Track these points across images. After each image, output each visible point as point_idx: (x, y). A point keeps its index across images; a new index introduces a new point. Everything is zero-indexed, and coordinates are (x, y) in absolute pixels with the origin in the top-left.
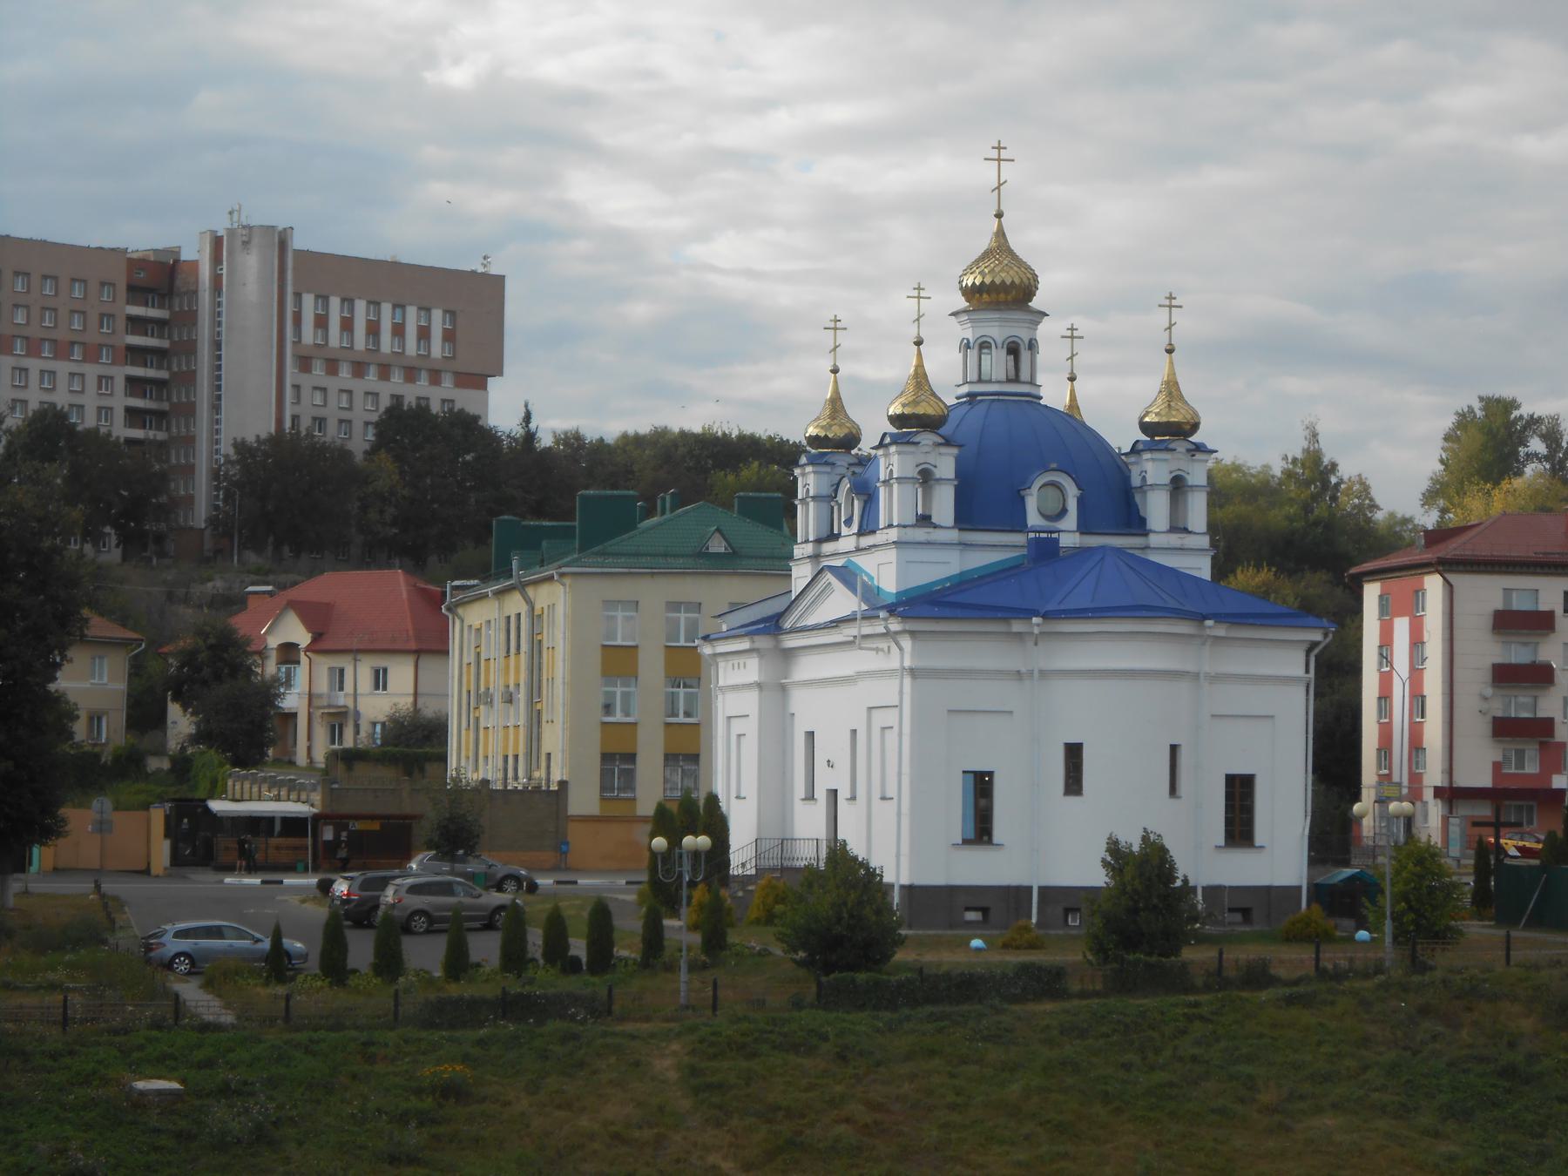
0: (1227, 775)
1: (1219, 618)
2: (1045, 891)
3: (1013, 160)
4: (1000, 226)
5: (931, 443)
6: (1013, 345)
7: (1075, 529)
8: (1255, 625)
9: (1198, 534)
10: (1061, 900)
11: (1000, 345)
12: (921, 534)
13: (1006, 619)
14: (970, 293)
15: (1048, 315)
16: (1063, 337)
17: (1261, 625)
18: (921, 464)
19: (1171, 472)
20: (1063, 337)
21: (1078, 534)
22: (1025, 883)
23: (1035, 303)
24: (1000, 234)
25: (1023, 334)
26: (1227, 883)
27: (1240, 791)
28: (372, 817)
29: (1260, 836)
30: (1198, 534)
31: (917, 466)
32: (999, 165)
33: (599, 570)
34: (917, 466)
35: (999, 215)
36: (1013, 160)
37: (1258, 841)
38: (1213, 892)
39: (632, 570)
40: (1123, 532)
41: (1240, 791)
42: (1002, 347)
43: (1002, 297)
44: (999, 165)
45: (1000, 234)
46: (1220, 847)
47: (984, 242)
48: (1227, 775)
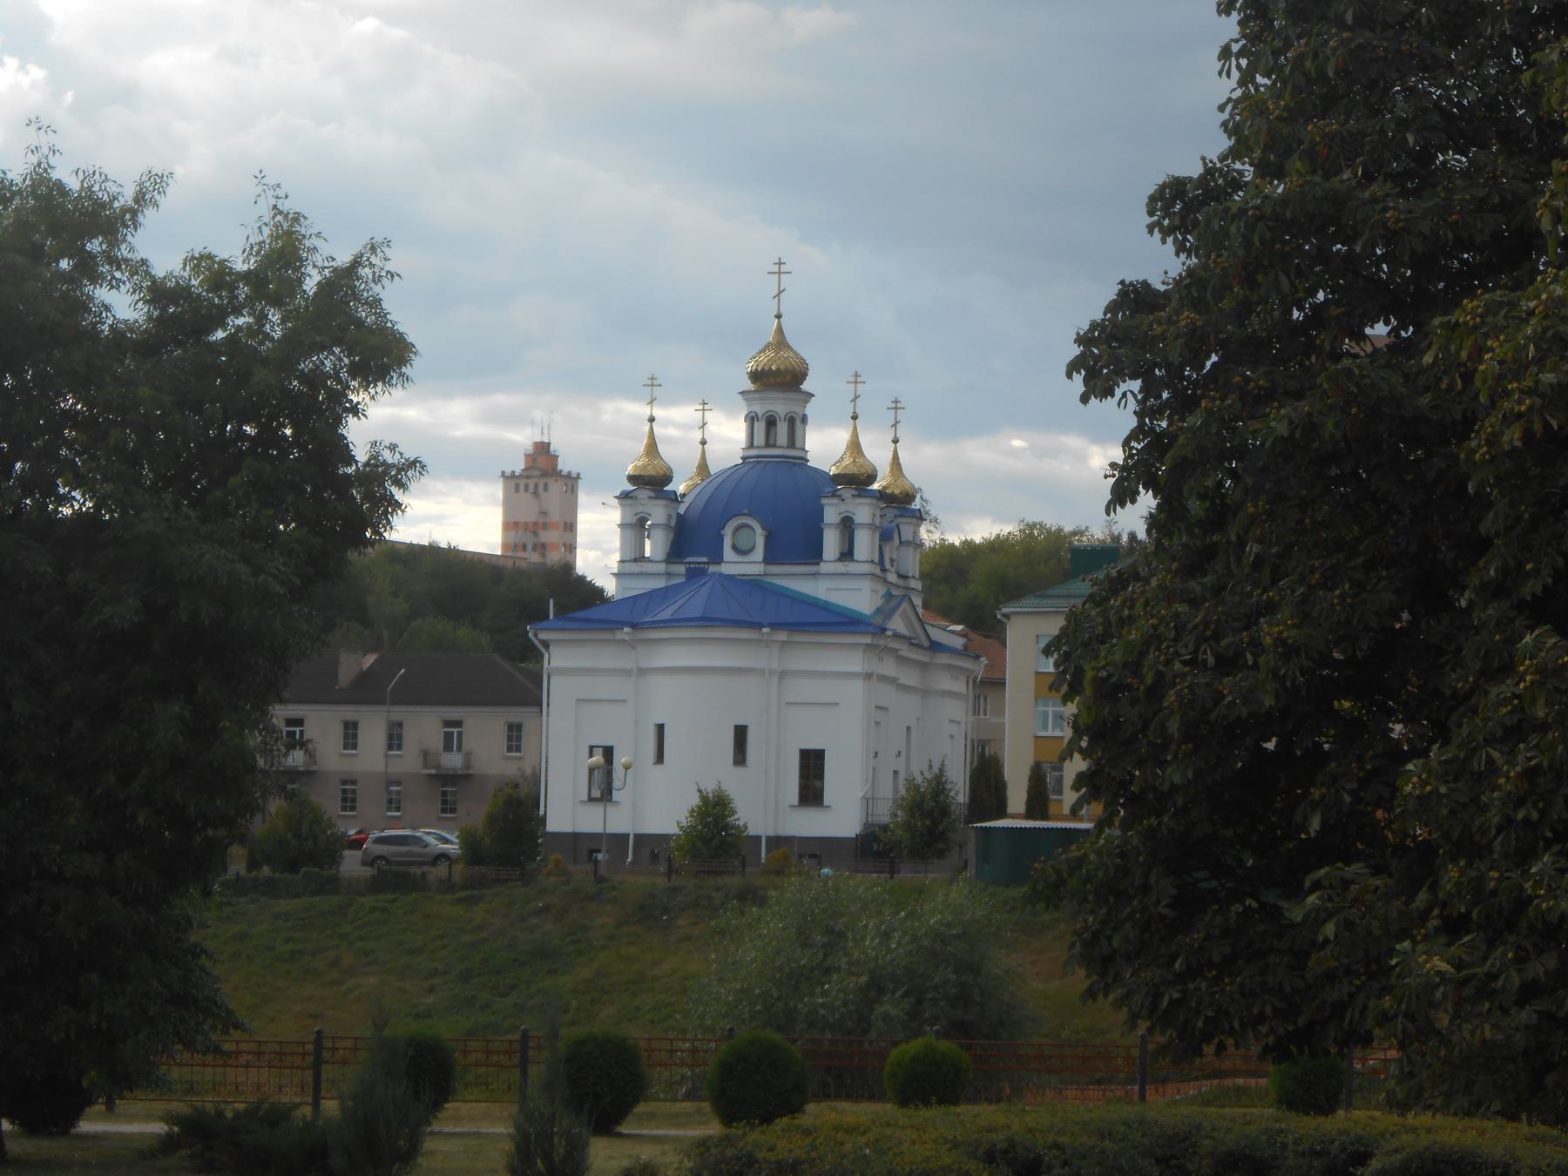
0: (823, 751)
1: (775, 626)
2: (640, 839)
3: (769, 273)
4: (779, 325)
5: (645, 497)
6: (772, 418)
7: (761, 560)
8: (809, 631)
9: (656, 562)
10: (651, 845)
11: (782, 419)
12: (635, 568)
13: (612, 630)
14: (755, 376)
15: (814, 396)
16: (888, 408)
17: (814, 632)
18: (640, 513)
19: (840, 514)
20: (888, 408)
21: (763, 565)
22: (627, 832)
23: (805, 386)
24: (780, 330)
25: (797, 409)
26: (798, 834)
27: (812, 764)
28: (545, 812)
29: (828, 798)
30: (656, 562)
31: (635, 515)
32: (775, 273)
33: (1030, 610)
34: (635, 515)
35: (779, 316)
36: (769, 273)
37: (826, 801)
38: (777, 842)
39: (1059, 609)
40: (800, 561)
41: (812, 764)
42: (785, 420)
43: (772, 380)
44: (775, 273)
45: (780, 330)
46: (794, 806)
47: (770, 337)
48: (823, 751)
